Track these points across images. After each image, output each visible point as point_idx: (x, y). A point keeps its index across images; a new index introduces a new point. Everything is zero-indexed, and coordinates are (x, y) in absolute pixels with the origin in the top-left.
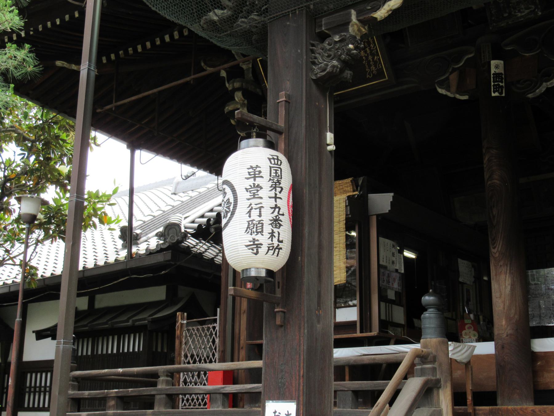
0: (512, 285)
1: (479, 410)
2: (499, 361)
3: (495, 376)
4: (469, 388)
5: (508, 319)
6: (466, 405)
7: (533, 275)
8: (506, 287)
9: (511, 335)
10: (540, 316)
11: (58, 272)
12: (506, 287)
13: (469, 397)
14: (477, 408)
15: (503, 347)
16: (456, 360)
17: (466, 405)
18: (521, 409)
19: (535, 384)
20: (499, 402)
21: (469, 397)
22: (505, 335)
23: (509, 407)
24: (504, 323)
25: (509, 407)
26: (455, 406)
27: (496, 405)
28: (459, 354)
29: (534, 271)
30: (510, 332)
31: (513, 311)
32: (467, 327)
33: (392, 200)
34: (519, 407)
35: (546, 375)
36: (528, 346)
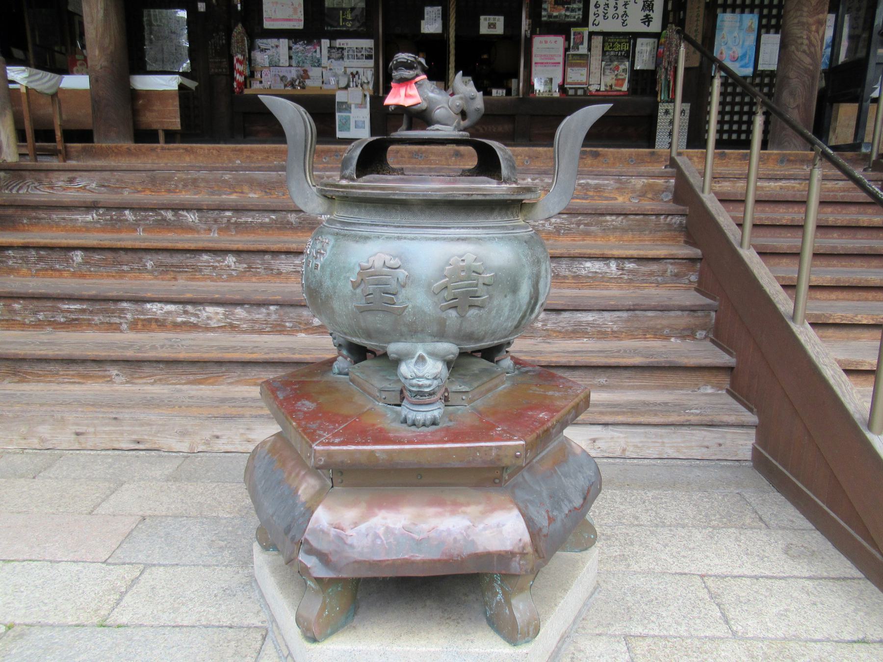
0: (106, 10)
1: (71, 147)
2: (94, 96)
3: (90, 111)
4: (57, 123)
5: (102, 49)
6: (54, 141)
7: (155, 16)
8: (98, 11)
9: (105, 67)
10: (163, 61)
11: (255, 392)
12: (98, 11)
13: (58, 134)
14: (68, 145)
15: (97, 81)
16: (35, 90)
17: (54, 141)
18: (116, 147)
19: (135, 124)
20: (95, 140)
21: (58, 134)
22: (98, 68)
23: (104, 145)
24: (97, 53)
25: (104, 145)
26: (37, 141)
27: (92, 142)
28: (38, 83)
29: (157, 10)
30: (105, 64)
31: (107, 41)
32: (78, 63)
33: (422, 22)
34: (114, 145)
35: (148, 114)
36: (128, 83)
